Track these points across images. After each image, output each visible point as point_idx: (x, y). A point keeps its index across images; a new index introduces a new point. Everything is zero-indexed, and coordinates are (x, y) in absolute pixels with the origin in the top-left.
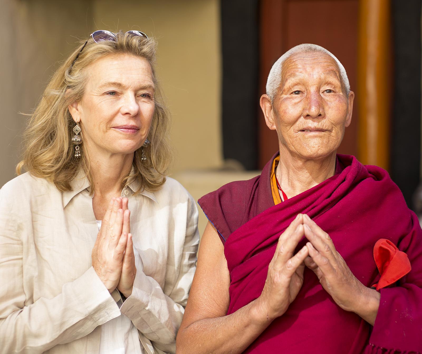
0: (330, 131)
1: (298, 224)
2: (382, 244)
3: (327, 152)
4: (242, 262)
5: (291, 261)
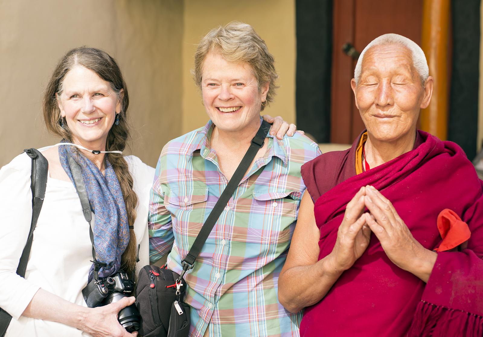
0: (399, 116)
1: (361, 196)
2: (444, 214)
3: (395, 136)
4: (326, 222)
5: (353, 226)
